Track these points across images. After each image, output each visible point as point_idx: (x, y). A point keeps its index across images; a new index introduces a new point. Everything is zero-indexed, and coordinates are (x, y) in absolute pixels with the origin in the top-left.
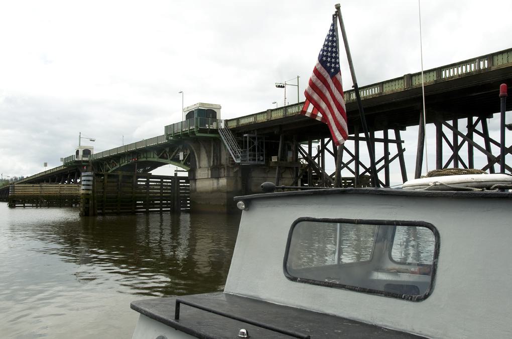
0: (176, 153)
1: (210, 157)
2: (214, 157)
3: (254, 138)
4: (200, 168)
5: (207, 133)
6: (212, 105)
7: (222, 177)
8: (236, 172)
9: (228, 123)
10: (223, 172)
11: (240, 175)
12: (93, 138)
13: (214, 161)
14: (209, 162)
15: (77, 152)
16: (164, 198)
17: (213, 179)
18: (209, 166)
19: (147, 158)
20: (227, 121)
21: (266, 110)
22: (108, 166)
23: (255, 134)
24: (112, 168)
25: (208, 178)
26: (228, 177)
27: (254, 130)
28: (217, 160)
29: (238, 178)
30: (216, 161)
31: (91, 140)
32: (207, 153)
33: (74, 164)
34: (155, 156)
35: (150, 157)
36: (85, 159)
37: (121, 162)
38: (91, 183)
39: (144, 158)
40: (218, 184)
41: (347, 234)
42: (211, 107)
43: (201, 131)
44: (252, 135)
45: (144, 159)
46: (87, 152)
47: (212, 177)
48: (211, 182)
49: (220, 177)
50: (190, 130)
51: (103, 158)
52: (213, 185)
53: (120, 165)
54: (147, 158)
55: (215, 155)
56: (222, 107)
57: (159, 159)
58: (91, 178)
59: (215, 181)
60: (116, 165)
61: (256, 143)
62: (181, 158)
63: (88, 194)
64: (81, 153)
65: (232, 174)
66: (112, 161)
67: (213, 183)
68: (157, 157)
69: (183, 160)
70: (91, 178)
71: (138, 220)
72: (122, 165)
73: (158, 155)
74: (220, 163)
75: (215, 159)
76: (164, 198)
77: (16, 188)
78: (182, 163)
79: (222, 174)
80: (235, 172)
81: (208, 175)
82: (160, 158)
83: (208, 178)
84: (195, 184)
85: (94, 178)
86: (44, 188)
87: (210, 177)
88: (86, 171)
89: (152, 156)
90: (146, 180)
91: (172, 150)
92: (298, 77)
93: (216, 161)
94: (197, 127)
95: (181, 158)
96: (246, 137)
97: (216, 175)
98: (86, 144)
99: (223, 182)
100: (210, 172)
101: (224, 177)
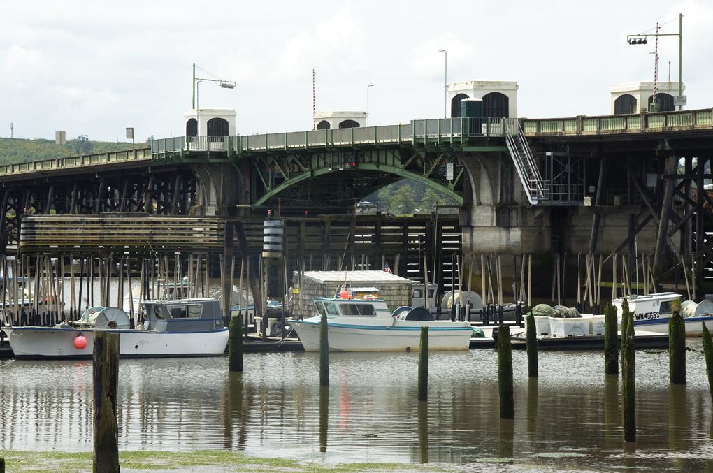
0: (441, 163)
1: (496, 184)
2: (502, 185)
3: (565, 160)
4: (479, 204)
5: (484, 145)
6: (499, 83)
7: (515, 227)
8: (540, 216)
9: (525, 124)
10: (515, 218)
11: (547, 222)
12: (229, 79)
13: (501, 195)
14: (494, 196)
15: (192, 126)
16: (410, 257)
17: (501, 228)
18: (495, 204)
19: (378, 163)
20: (523, 122)
21: (575, 116)
22: (277, 168)
23: (566, 151)
24: (292, 176)
25: (492, 226)
26: (523, 226)
27: (565, 144)
28: (507, 192)
29: (543, 228)
30: (505, 194)
31: (224, 86)
32: (489, 177)
33: (185, 161)
34: (397, 163)
35: (386, 164)
36: (216, 146)
37: (315, 165)
38: (279, 239)
39: (371, 162)
40: (508, 239)
41: (26, 272)
42: (497, 87)
43: (471, 142)
44: (559, 154)
45: (373, 167)
46: (218, 127)
47: (499, 224)
48: (498, 234)
49: (512, 227)
50: (453, 138)
51: (268, 150)
52: (500, 240)
53: (312, 172)
54: (378, 163)
55: (504, 182)
56: (520, 87)
57: (405, 172)
58: (280, 231)
59: (504, 233)
60: (301, 172)
61: (568, 168)
62: (450, 175)
63: (275, 259)
64: (202, 130)
65: (531, 222)
66: (290, 159)
67: (500, 236)
68: (401, 166)
69: (453, 181)
70: (280, 231)
71: (574, 223)
72: (318, 173)
73: (403, 162)
74: (512, 199)
75: (504, 191)
76: (410, 257)
77: (36, 226)
78: (452, 186)
79: (514, 222)
80: (537, 218)
81: (492, 221)
82: (407, 169)
83: (492, 226)
84: (472, 236)
85: (284, 229)
86: (111, 225)
87: (495, 224)
88: (271, 219)
89: (390, 161)
90: (374, 228)
91: (432, 156)
92: (681, 16)
93: (505, 194)
94: (464, 136)
95: (450, 175)
96: (549, 157)
97: (503, 223)
98: (214, 103)
99: (516, 234)
100: (495, 214)
101: (518, 226)
